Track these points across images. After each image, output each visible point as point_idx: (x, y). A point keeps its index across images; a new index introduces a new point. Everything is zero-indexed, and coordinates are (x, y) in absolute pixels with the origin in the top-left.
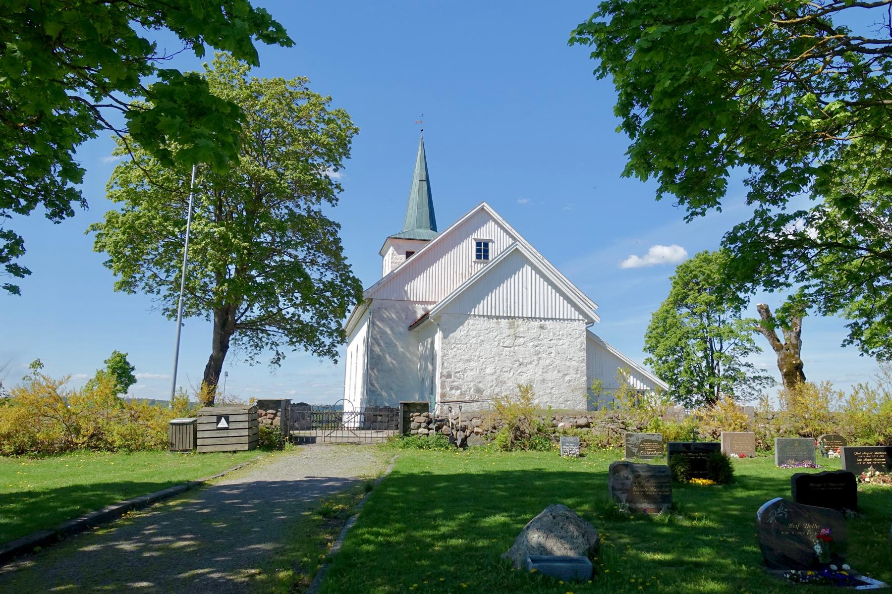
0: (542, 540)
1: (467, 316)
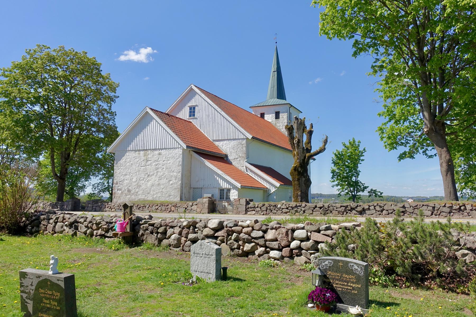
1: (126, 151)
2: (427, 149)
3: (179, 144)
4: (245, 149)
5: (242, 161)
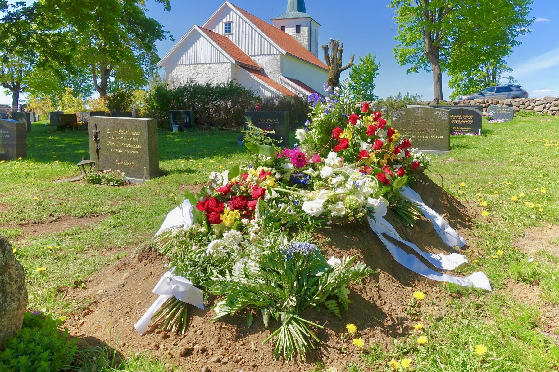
0: (449, 230)
1: (176, 65)
2: (427, 65)
3: (228, 59)
5: (277, 75)
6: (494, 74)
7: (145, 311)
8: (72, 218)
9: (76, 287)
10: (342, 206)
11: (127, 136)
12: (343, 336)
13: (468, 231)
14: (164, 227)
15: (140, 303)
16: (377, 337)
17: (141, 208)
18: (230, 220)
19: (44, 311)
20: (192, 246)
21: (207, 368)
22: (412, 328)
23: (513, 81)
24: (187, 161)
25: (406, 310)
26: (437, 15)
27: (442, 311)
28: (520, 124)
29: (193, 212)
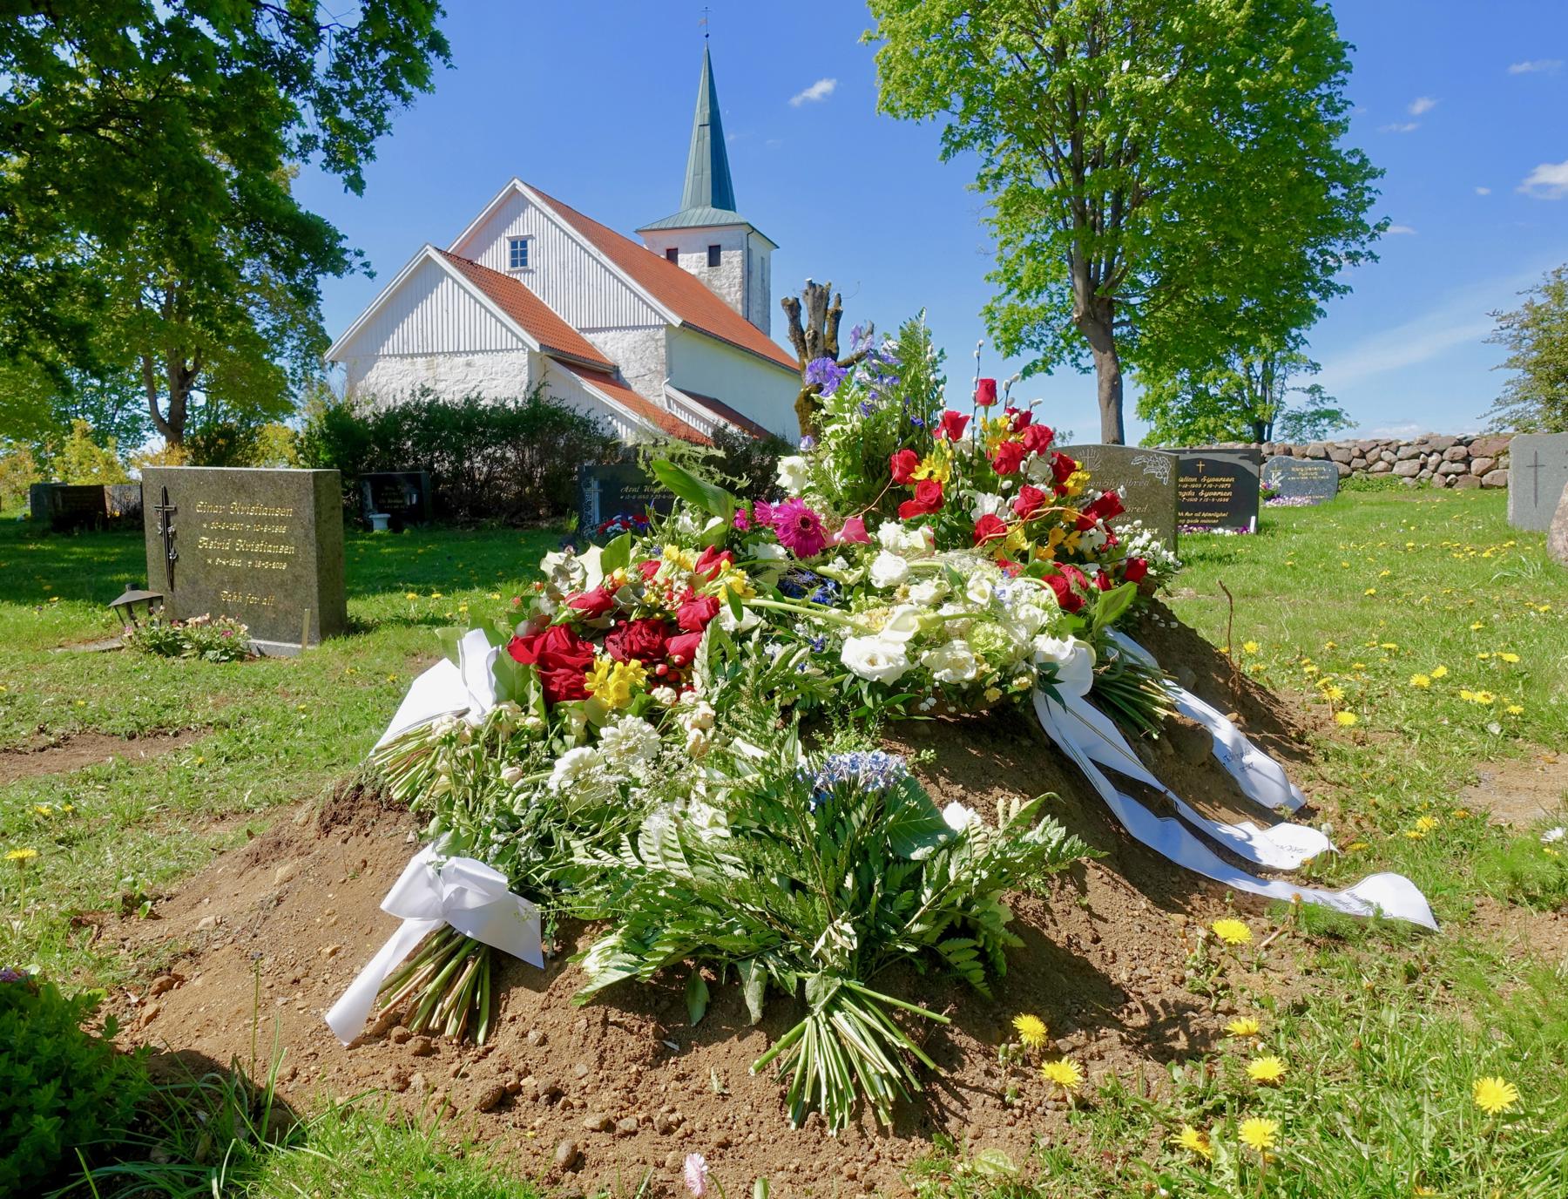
0: (1254, 757)
1: (376, 359)
3: (519, 339)
4: (662, 351)
5: (655, 383)
6: (1268, 378)
7: (353, 975)
8: (102, 738)
9: (129, 913)
10: (966, 654)
11: (259, 521)
12: (1006, 1054)
13: (1308, 770)
14: (405, 719)
15: (334, 953)
16: (1112, 1063)
17: (304, 711)
18: (618, 689)
19: (34, 970)
20: (498, 771)
21: (575, 1147)
22: (1222, 1035)
23: (1322, 399)
24: (424, 599)
25: (1183, 980)
26: (1108, 212)
27: (1294, 986)
28: (1360, 509)
29: (498, 668)
